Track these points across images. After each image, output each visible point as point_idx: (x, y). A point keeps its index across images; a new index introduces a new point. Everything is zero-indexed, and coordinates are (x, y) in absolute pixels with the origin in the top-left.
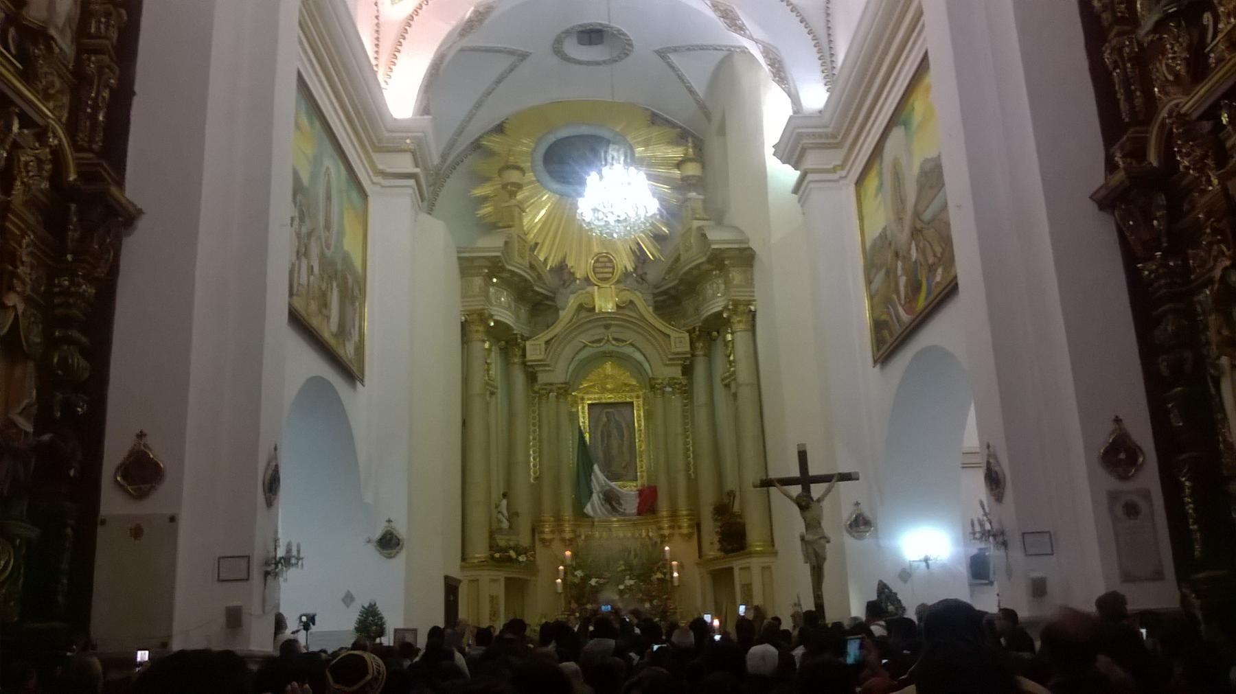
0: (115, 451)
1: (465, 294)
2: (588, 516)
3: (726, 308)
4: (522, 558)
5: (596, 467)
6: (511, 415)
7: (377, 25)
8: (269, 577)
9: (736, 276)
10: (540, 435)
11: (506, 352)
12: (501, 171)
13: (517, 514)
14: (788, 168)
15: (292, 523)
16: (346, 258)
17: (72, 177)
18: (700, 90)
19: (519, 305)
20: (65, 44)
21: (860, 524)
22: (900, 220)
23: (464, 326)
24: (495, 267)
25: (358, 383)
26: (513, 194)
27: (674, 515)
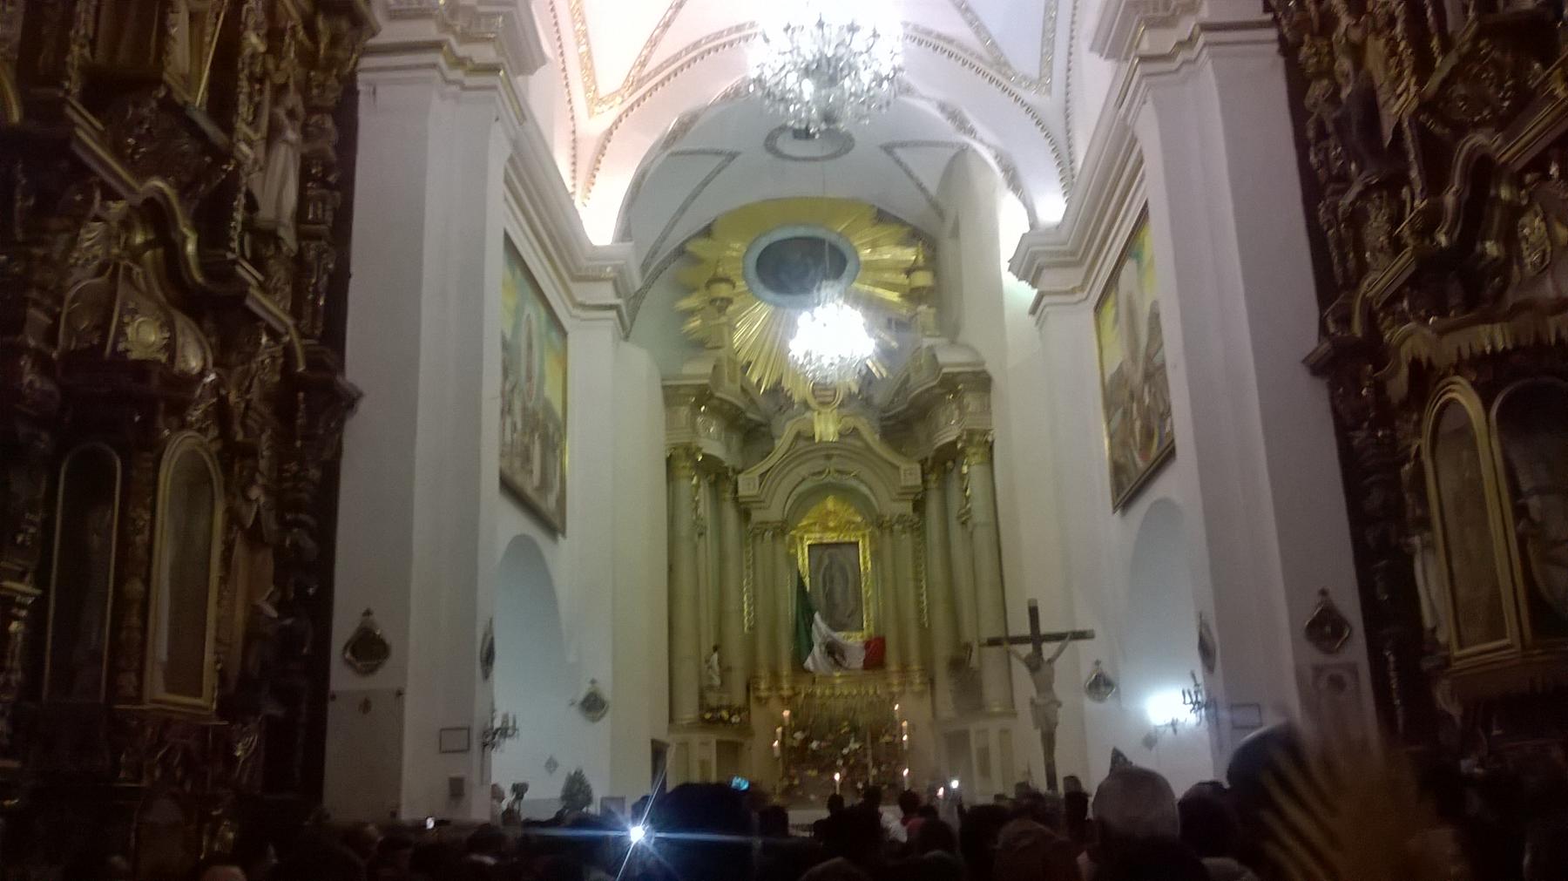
0: (343, 628)
1: (670, 426)
2: (807, 671)
3: (959, 438)
4: (735, 719)
5: (817, 616)
6: (722, 558)
7: (574, 140)
8: (487, 749)
9: (971, 401)
10: (754, 580)
11: (715, 486)
12: (709, 284)
13: (729, 669)
14: (1024, 285)
15: (510, 693)
16: (548, 407)
17: (301, 369)
18: (932, 188)
19: (732, 433)
20: (288, 237)
21: (1101, 685)
22: (1134, 358)
23: (670, 461)
24: (703, 395)
25: (560, 537)
26: (722, 310)
27: (904, 669)
